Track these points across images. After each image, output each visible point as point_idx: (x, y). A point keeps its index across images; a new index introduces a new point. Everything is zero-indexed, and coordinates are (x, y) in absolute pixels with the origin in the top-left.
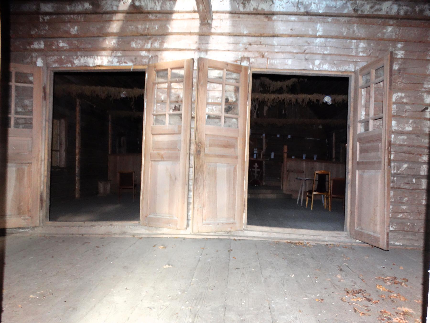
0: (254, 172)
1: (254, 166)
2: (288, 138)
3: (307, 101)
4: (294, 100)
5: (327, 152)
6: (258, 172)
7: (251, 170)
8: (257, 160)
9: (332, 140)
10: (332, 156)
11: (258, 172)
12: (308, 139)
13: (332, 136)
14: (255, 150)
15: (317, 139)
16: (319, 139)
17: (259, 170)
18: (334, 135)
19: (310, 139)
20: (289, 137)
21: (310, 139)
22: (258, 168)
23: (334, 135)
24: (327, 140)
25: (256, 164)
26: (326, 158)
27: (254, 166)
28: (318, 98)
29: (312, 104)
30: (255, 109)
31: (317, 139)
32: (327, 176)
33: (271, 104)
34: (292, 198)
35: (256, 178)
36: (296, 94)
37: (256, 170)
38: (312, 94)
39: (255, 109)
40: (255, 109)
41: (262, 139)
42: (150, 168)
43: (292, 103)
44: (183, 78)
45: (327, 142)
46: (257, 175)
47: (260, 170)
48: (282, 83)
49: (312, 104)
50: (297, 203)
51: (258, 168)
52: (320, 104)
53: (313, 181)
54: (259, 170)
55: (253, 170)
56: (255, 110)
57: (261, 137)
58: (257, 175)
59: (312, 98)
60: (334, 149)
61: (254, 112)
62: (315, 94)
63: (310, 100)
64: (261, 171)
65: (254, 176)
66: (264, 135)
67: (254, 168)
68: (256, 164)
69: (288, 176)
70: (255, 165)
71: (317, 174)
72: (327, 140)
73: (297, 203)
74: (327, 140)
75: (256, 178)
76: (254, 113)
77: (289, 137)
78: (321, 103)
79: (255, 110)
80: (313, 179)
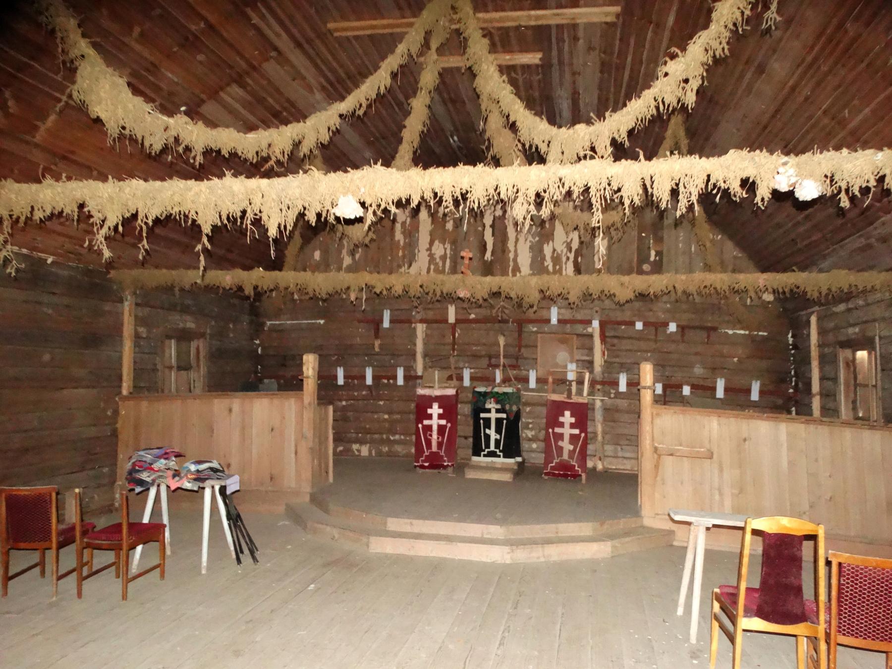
0: (560, 437)
1: (561, 419)
2: (668, 332)
3: (692, 191)
4: (632, 193)
5: (793, 373)
6: (574, 439)
7: (550, 430)
8: (571, 401)
9: (809, 335)
10: (809, 385)
11: (574, 439)
12: (730, 332)
13: (808, 323)
14: (370, 451)
15: (760, 333)
16: (765, 334)
17: (576, 431)
18: (813, 319)
19: (738, 332)
20: (673, 327)
21: (738, 332)
22: (572, 426)
23: (813, 319)
24: (790, 335)
25: (567, 413)
26: (791, 391)
27: (561, 419)
28: (750, 172)
29: (717, 199)
30: (570, 250)
31: (760, 333)
32: (807, 546)
33: (528, 212)
34: (675, 543)
35: (565, 456)
36: (642, 157)
37: (567, 431)
38: (721, 151)
39: (570, 250)
40: (570, 252)
41: (591, 336)
42: (29, 488)
43: (627, 202)
44: (730, 268)
45: (791, 340)
46: (571, 447)
47: (581, 432)
48: (592, 128)
49: (717, 199)
50: (680, 611)
51: (572, 426)
52: (758, 199)
53: (741, 532)
54: (576, 431)
55: (558, 430)
56: (569, 254)
57: (590, 330)
58: (571, 447)
59: (718, 176)
60: (815, 364)
61: (568, 259)
62: (732, 151)
63: (712, 181)
64: (583, 435)
65: (560, 449)
66: (596, 324)
67: (562, 425)
68: (567, 413)
69: (657, 467)
70: (563, 415)
71: (755, 532)
72: (790, 335)
73: (680, 611)
74: (792, 337)
75: (565, 456)
76: (566, 263)
77: (673, 327)
78: (767, 196)
79: (569, 254)
80: (742, 524)
